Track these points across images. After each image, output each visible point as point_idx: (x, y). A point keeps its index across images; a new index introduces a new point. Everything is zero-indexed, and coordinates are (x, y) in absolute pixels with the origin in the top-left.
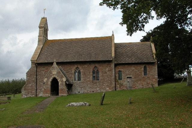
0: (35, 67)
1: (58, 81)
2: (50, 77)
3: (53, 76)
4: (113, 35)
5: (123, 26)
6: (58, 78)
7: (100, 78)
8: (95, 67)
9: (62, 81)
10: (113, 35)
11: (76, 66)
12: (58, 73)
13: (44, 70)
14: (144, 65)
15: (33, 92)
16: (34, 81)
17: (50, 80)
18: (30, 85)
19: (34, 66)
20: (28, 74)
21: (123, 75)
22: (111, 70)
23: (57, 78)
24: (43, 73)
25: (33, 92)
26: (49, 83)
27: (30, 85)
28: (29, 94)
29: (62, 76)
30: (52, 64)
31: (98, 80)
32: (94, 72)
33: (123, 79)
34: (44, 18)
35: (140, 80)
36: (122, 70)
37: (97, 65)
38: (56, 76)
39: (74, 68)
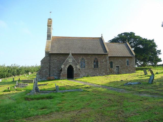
0: (48, 56)
1: (73, 67)
2: (67, 65)
3: (69, 64)
4: (102, 37)
5: (161, 54)
6: (73, 65)
7: (99, 66)
8: (96, 58)
9: (76, 68)
10: (102, 37)
11: (82, 57)
12: (73, 61)
13: (57, 59)
14: (82, 57)
15: (46, 76)
16: (48, 67)
17: (67, 67)
18: (44, 70)
19: (48, 55)
20: (43, 61)
21: (113, 65)
22: (106, 61)
23: (72, 65)
24: (56, 61)
25: (46, 76)
26: (66, 69)
27: (44, 70)
28: (43, 77)
29: (77, 64)
30: (68, 54)
31: (98, 67)
32: (94, 62)
33: (113, 67)
34: (50, 19)
35: (124, 68)
36: (113, 61)
37: (97, 57)
38: (72, 64)
39: (80, 58)
